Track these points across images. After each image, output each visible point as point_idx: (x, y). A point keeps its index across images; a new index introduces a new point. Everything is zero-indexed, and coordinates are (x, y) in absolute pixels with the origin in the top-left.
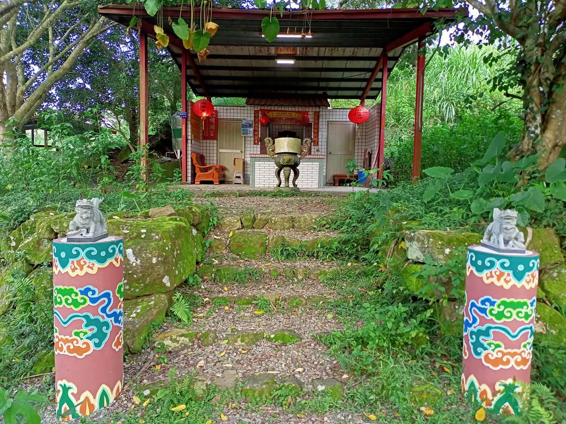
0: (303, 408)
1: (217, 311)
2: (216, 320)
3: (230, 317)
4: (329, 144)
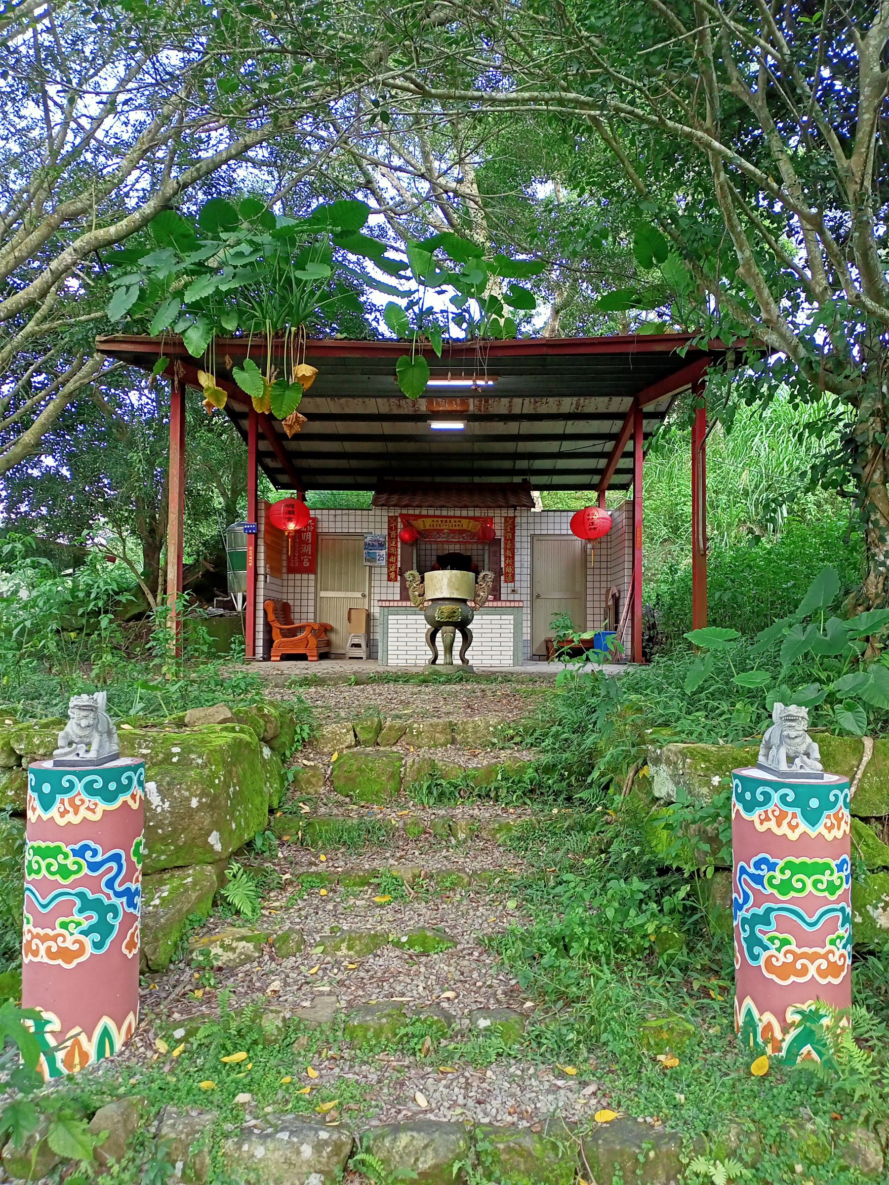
0: (451, 1056)
1: (306, 897)
2: (303, 913)
3: (330, 907)
4: (536, 579)
